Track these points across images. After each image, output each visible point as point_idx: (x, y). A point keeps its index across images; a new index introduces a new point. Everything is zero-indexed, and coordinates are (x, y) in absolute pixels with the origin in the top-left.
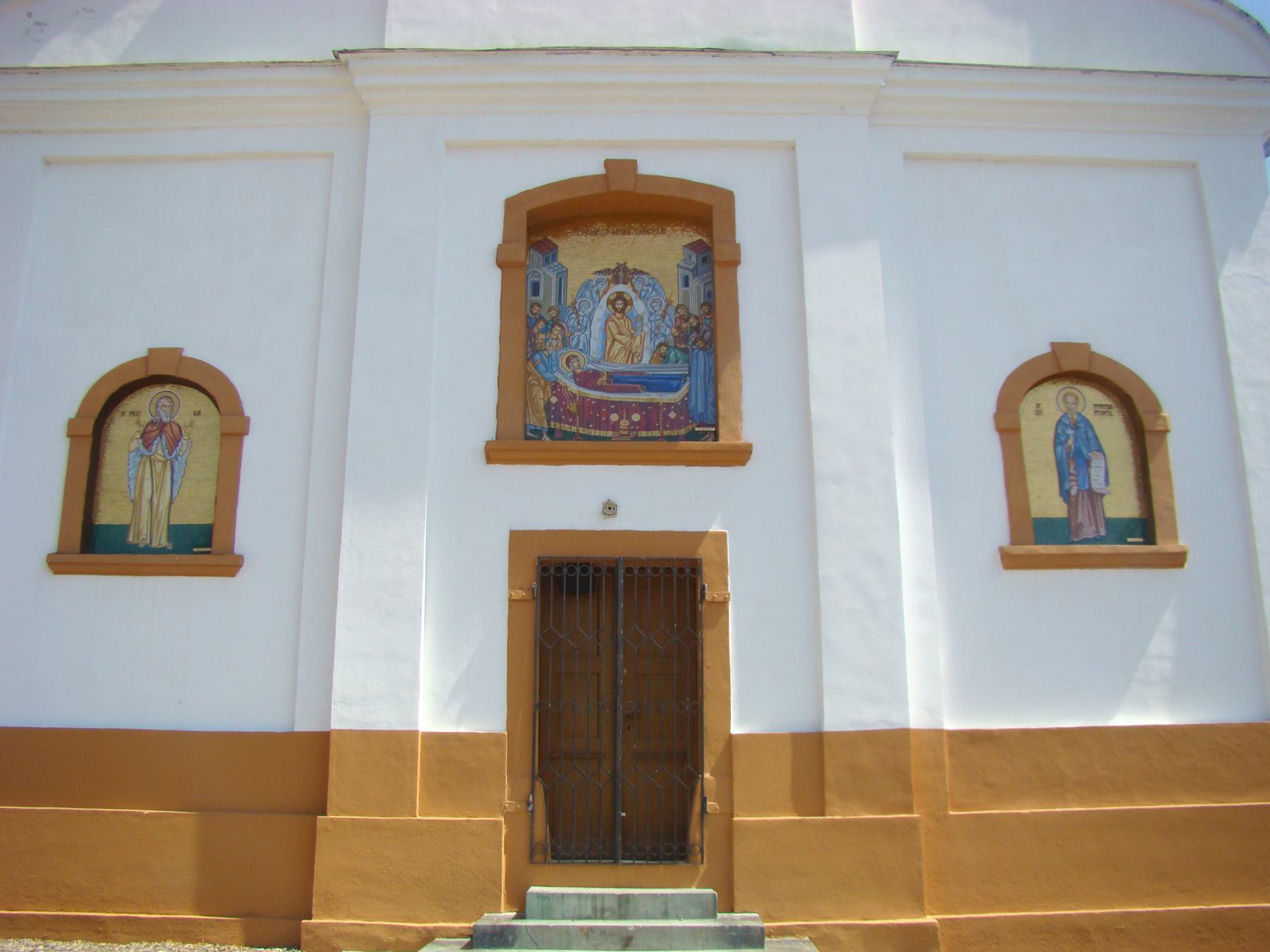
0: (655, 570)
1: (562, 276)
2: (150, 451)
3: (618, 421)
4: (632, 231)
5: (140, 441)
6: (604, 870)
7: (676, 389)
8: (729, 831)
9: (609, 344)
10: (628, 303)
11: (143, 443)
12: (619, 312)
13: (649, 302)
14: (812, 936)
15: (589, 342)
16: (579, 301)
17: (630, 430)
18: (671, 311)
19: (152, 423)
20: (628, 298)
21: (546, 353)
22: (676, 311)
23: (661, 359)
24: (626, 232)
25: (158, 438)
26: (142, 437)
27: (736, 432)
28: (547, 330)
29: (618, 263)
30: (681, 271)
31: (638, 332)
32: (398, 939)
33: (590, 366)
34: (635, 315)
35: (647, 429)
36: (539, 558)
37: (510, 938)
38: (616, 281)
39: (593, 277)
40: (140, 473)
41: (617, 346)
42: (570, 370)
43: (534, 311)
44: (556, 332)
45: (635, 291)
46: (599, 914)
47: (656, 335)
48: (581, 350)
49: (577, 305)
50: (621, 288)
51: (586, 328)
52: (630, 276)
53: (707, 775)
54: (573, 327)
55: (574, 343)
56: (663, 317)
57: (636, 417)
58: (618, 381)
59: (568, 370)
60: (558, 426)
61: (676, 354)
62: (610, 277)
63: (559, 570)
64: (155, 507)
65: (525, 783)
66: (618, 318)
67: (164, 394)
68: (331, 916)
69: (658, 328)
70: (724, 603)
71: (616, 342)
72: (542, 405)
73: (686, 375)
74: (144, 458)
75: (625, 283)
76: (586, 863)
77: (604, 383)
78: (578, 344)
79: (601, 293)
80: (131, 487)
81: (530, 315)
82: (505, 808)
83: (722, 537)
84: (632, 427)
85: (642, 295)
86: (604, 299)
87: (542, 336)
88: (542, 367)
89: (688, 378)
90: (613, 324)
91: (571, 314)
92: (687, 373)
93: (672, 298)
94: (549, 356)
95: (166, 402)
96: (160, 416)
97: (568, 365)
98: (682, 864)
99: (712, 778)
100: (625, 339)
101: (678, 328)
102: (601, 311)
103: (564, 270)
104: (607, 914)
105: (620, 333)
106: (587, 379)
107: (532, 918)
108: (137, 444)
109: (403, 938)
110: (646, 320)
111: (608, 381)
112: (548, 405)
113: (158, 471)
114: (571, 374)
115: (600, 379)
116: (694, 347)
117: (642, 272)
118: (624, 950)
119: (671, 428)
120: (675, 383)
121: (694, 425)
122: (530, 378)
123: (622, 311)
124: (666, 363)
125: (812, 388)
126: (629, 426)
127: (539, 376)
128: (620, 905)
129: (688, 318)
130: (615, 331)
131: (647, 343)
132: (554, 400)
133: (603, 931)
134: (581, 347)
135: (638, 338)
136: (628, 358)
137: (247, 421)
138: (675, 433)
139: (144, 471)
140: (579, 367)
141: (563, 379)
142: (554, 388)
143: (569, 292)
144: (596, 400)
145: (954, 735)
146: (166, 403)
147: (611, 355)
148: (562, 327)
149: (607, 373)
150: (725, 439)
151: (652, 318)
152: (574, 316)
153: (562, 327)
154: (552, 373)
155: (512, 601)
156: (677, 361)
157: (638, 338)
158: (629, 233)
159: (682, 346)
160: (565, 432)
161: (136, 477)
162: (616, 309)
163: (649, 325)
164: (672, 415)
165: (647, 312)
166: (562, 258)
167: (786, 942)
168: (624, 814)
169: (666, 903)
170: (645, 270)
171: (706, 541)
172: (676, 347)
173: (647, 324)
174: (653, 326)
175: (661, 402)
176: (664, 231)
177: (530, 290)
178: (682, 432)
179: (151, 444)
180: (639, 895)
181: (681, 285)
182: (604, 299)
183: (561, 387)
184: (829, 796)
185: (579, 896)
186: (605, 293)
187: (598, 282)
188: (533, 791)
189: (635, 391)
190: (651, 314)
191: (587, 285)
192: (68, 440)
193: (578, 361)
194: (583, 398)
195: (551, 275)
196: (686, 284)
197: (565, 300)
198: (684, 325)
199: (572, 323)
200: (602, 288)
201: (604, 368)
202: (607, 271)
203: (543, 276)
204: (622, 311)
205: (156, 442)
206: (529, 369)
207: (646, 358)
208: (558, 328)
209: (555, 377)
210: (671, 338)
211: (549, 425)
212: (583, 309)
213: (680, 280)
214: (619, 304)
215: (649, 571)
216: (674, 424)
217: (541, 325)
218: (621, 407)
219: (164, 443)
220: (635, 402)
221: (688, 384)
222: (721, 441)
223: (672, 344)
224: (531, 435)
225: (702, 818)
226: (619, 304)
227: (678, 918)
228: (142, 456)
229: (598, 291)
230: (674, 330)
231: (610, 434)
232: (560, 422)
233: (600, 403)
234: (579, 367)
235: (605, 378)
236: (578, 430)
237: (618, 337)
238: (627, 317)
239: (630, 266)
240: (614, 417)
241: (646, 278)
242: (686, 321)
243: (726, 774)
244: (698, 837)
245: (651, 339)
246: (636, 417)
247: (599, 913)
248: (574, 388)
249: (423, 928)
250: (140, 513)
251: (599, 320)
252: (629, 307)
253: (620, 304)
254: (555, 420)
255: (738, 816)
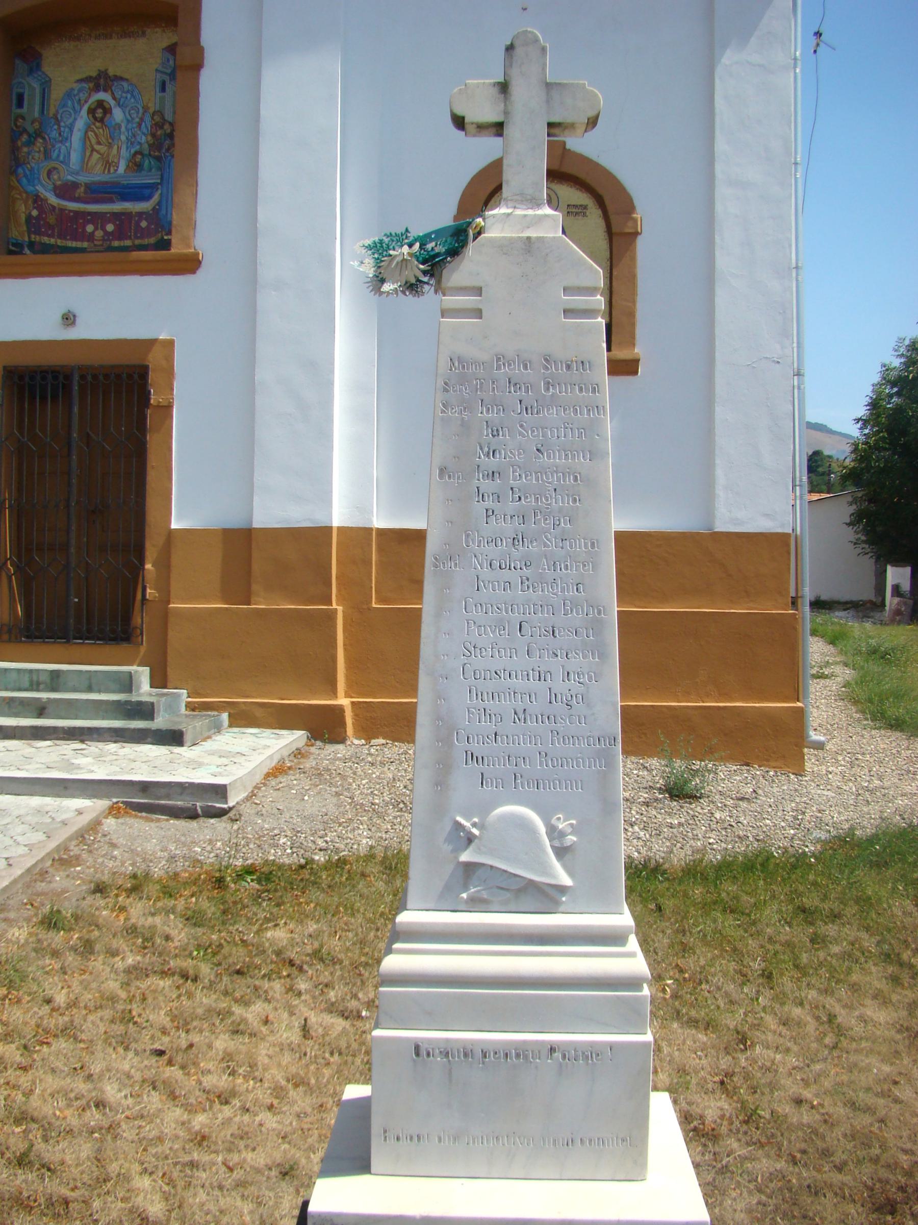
0: (106, 376)
1: (46, 85)
3: (93, 232)
4: (114, 35)
6: (58, 649)
7: (148, 198)
8: (165, 615)
9: (88, 154)
10: (107, 111)
12: (99, 122)
13: (128, 109)
14: (232, 712)
15: (69, 153)
17: (104, 240)
18: (148, 119)
20: (107, 106)
21: (29, 166)
22: (152, 118)
23: (135, 168)
24: (108, 36)
27: (187, 241)
28: (30, 143)
29: (99, 70)
30: (159, 75)
31: (116, 142)
33: (70, 178)
34: (113, 123)
35: (120, 239)
38: (97, 88)
39: (77, 86)
41: (96, 156)
42: (50, 183)
43: (18, 124)
44: (38, 144)
45: (114, 98)
46: (35, 687)
47: (132, 143)
48: (61, 162)
49: (59, 117)
50: (101, 96)
51: (67, 139)
52: (110, 83)
53: (148, 566)
54: (55, 139)
55: (55, 155)
56: (140, 125)
57: (110, 228)
58: (99, 192)
59: (48, 181)
60: (38, 238)
61: (150, 162)
62: (91, 85)
63: (32, 378)
66: (97, 128)
69: (134, 136)
70: (169, 407)
71: (95, 153)
73: (158, 184)
75: (105, 90)
76: (44, 642)
77: (82, 195)
78: (58, 156)
79: (82, 102)
81: (15, 128)
83: (170, 344)
84: (106, 238)
85: (121, 103)
86: (86, 107)
87: (25, 150)
88: (24, 181)
89: (160, 187)
90: (92, 134)
91: (54, 125)
92: (159, 181)
93: (150, 105)
94: (32, 170)
97: (49, 178)
98: (125, 645)
99: (152, 568)
100: (102, 149)
101: (153, 135)
102: (82, 121)
103: (47, 79)
104: (42, 686)
105: (99, 143)
106: (66, 191)
110: (123, 129)
111: (85, 192)
112: (29, 218)
114: (51, 187)
115: (78, 191)
116: (167, 154)
117: (122, 79)
118: (38, 718)
119: (142, 237)
120: (147, 192)
121: (164, 233)
122: (14, 192)
123: (102, 120)
124: (140, 171)
125: (261, 194)
126: (103, 237)
127: (22, 190)
128: (52, 679)
129: (163, 125)
130: (94, 141)
131: (124, 152)
132: (35, 213)
133: (23, 702)
134: (61, 158)
135: (115, 147)
136: (105, 167)
138: (146, 241)
140: (59, 179)
141: (44, 192)
142: (35, 202)
143: (52, 102)
145: (383, 533)
147: (90, 164)
148: (43, 138)
149: (86, 184)
150: (177, 249)
151: (130, 126)
152: (56, 127)
153: (43, 138)
154: (34, 186)
156: (150, 170)
157: (115, 147)
158: (111, 38)
159: (156, 154)
162: (95, 119)
163: (126, 133)
164: (144, 224)
165: (125, 121)
166: (48, 68)
167: (209, 715)
168: (76, 600)
169: (90, 679)
170: (126, 76)
171: (156, 348)
172: (150, 155)
173: (124, 133)
174: (130, 133)
175: (134, 211)
176: (144, 34)
177: (14, 102)
178: (152, 240)
180: (68, 671)
181: (158, 91)
182: (86, 107)
183: (42, 200)
184: (255, 587)
185: (19, 671)
186: (86, 102)
187: (80, 91)
189: (111, 201)
190: (128, 121)
191: (69, 94)
193: (58, 173)
194: (62, 210)
195: (35, 86)
196: (163, 89)
197: (48, 110)
198: (159, 133)
199: (54, 134)
200: (83, 96)
201: (83, 179)
202: (88, 79)
203: (27, 86)
204: (102, 120)
206: (12, 183)
207: (122, 169)
208: (41, 141)
209: (37, 190)
210: (146, 146)
211: (29, 237)
212: (65, 120)
213: (158, 84)
214: (99, 113)
215: (101, 378)
216: (143, 233)
217: (25, 137)
218: (98, 219)
220: (109, 213)
221: (159, 192)
222: (173, 251)
223: (146, 152)
224: (13, 248)
225: (143, 604)
226: (99, 113)
227: (99, 691)
229: (80, 100)
230: (150, 138)
231: (85, 245)
232: (39, 235)
233: (77, 214)
234: (59, 179)
235: (82, 189)
236: (56, 242)
237: (97, 147)
238: (106, 126)
239: (111, 72)
240: (90, 228)
241: (125, 84)
242: (162, 127)
243: (164, 564)
244: (139, 621)
245: (127, 148)
246: (110, 228)
247: (35, 686)
248: (53, 200)
251: (79, 130)
252: (108, 116)
253: (100, 112)
254: (35, 233)
255: (174, 603)
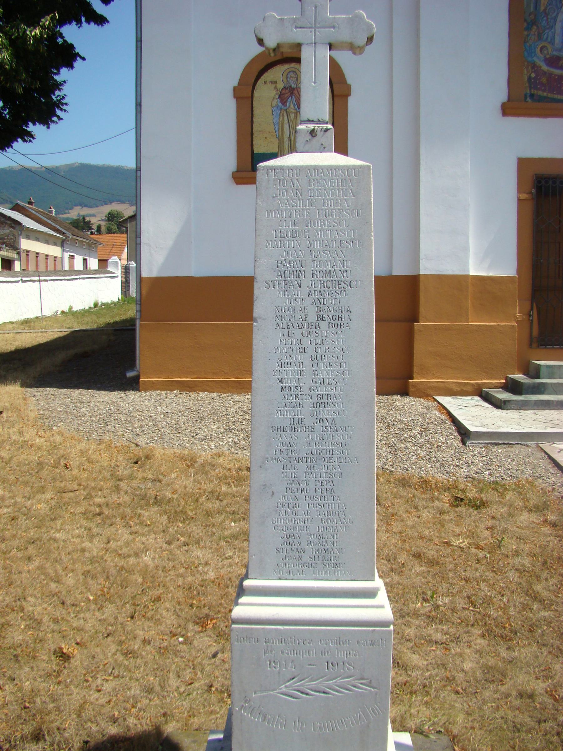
2: (286, 106)
5: (279, 100)
11: (280, 101)
16: (548, 8)
19: (285, 88)
25: (290, 98)
26: (279, 97)
32: (462, 390)
36: (536, 175)
37: (543, 389)
40: (281, 120)
51: (552, 27)
55: (545, 37)
60: (536, 92)
64: (292, 142)
65: (527, 305)
67: (291, 70)
68: (424, 378)
72: (526, 78)
74: (282, 111)
76: (560, 348)
78: (547, 38)
80: (276, 129)
82: (517, 318)
95: (292, 75)
96: (289, 83)
97: (542, 53)
107: (544, 378)
108: (277, 102)
109: (464, 389)
112: (530, 78)
113: (292, 119)
114: (543, 59)
132: (533, 75)
134: (549, 40)
137: (349, 87)
139: (283, 119)
142: (533, 68)
144: (559, 76)
146: (293, 75)
155: (519, 200)
160: (540, 96)
161: (279, 123)
179: (286, 102)
188: (532, 309)
192: (235, 100)
194: (551, 74)
199: (544, 23)
205: (289, 100)
219: (294, 101)
228: (281, 109)
248: (545, 68)
249: (476, 383)
250: (283, 146)
